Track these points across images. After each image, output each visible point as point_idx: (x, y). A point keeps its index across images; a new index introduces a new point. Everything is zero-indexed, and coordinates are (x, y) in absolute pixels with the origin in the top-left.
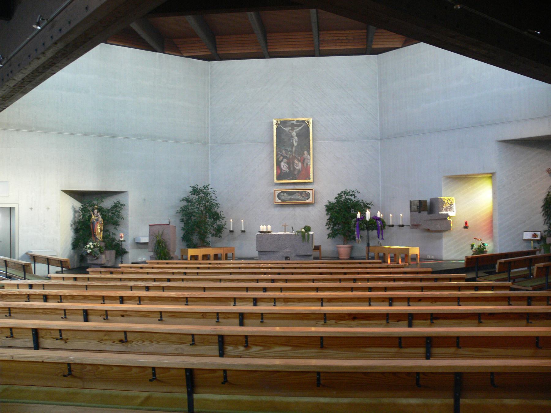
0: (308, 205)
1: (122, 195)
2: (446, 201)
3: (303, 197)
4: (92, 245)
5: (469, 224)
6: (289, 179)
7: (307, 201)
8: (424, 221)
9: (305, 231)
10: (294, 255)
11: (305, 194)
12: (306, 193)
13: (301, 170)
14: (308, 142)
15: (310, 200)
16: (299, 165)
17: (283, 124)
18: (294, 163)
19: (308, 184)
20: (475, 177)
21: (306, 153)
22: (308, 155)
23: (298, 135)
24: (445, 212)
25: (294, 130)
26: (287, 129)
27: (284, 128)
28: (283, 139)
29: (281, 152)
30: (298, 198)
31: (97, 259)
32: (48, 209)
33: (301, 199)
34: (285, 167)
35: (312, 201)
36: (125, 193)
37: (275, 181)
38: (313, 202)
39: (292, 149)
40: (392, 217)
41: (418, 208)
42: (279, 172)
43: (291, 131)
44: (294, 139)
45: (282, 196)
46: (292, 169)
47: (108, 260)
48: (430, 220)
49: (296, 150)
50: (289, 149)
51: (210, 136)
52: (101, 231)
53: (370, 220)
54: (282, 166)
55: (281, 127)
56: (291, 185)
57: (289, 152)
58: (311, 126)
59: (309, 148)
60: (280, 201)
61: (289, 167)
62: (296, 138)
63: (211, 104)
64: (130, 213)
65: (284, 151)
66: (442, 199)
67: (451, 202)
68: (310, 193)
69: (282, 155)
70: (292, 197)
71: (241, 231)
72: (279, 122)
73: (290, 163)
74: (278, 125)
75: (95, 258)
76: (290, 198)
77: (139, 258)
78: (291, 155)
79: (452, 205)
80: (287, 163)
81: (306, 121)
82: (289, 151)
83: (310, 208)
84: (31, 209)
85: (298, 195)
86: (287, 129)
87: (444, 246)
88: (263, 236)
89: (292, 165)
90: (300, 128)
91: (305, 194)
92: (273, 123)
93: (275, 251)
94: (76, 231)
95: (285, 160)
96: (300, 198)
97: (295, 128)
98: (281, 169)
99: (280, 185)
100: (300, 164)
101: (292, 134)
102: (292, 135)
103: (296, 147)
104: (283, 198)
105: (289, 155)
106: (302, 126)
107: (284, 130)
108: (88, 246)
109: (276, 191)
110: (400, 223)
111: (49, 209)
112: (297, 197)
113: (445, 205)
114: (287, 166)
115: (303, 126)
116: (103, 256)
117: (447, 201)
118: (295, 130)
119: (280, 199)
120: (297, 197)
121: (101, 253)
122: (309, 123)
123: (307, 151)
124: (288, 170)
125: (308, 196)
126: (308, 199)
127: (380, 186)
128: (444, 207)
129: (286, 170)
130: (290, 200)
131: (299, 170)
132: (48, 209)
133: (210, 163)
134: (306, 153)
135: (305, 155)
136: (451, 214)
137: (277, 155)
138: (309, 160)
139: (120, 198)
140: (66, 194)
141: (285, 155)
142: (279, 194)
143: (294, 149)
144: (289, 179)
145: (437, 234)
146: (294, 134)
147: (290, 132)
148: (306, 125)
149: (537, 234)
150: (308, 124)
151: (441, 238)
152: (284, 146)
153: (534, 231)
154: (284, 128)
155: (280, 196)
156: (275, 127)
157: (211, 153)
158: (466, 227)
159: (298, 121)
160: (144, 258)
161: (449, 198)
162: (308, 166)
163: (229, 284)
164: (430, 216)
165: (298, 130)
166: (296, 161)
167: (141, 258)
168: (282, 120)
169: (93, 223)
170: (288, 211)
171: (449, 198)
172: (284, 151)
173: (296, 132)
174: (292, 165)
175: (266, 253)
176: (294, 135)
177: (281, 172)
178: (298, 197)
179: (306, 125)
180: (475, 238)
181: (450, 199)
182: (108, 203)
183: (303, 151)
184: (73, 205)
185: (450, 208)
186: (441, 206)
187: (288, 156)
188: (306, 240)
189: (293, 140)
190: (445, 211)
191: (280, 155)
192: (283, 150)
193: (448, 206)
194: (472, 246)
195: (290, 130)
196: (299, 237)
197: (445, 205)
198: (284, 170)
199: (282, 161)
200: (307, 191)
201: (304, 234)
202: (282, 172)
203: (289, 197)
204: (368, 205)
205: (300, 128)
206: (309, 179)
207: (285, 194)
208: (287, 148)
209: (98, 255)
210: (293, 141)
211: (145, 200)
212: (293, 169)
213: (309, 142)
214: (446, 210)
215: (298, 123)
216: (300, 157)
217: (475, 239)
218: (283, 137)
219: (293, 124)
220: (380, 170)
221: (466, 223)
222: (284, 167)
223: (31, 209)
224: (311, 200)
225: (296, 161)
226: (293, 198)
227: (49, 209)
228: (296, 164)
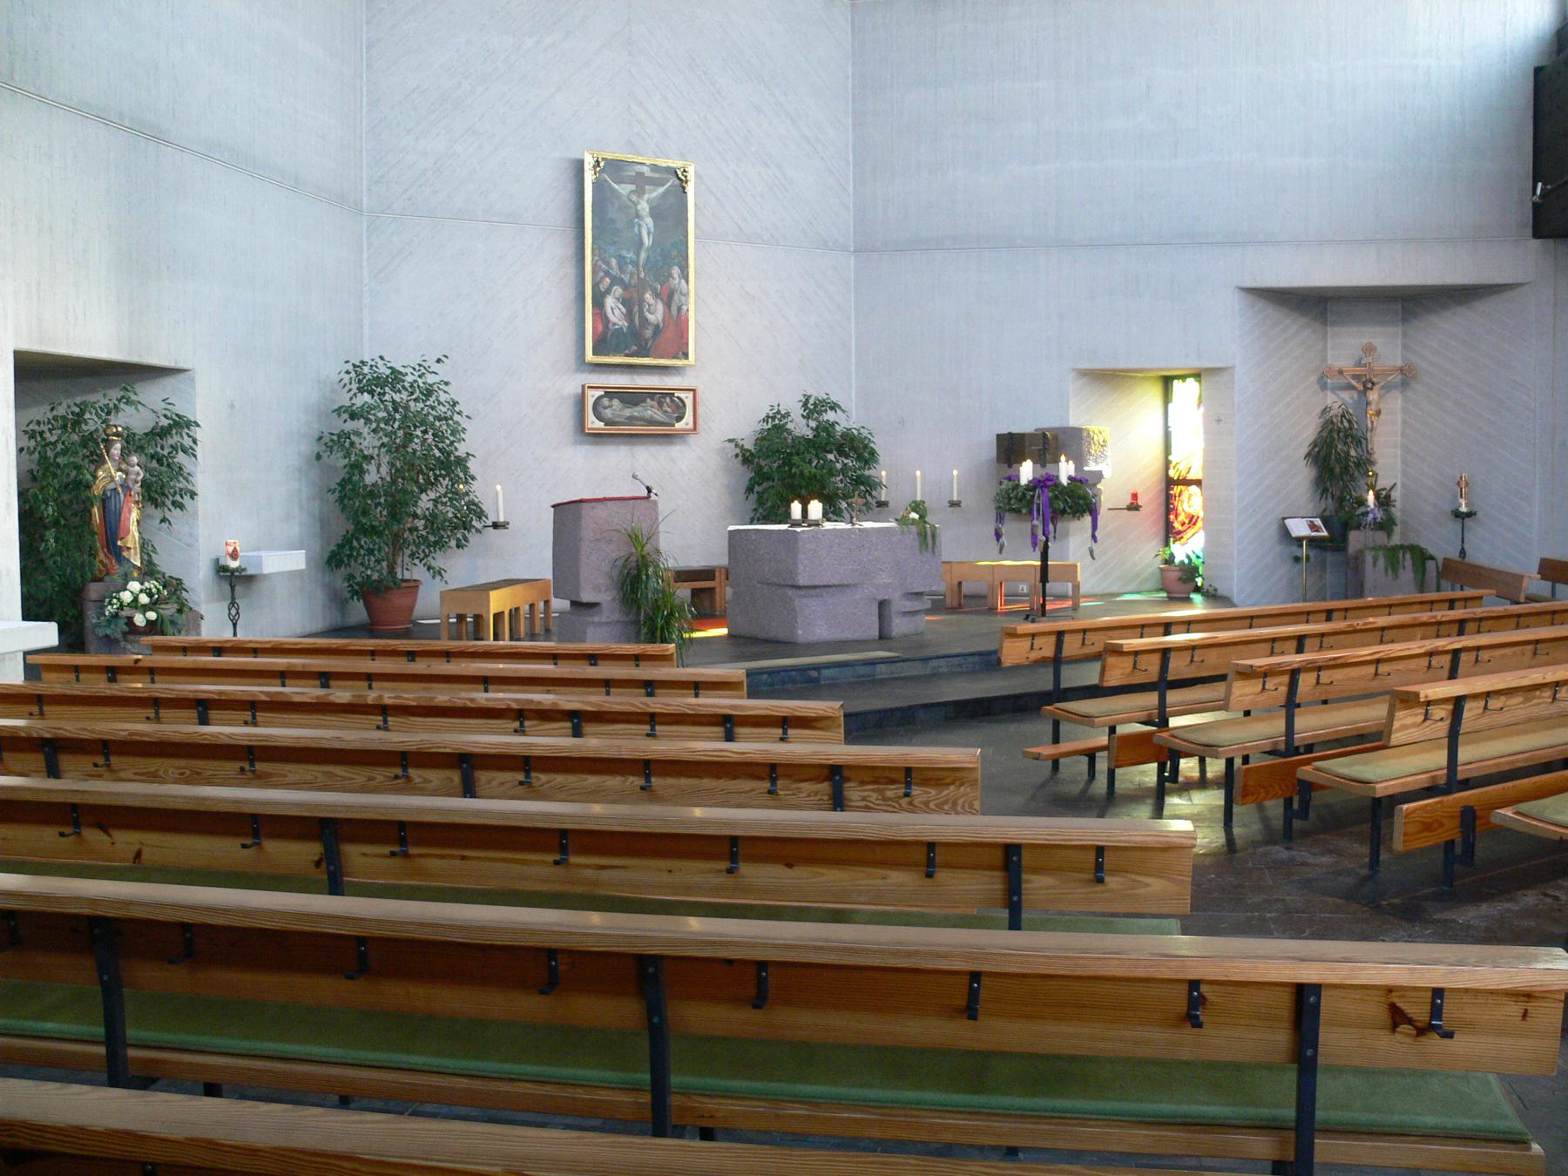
0: (669, 438)
3: (666, 412)
7: (678, 425)
21: (676, 271)
22: (683, 281)
23: (655, 213)
26: (624, 189)
28: (612, 221)
29: (608, 264)
30: (651, 417)
36: (182, 376)
37: (590, 356)
39: (638, 255)
43: (634, 198)
45: (605, 408)
49: (648, 259)
50: (630, 255)
55: (606, 181)
58: (690, 189)
60: (601, 425)
62: (649, 221)
70: (636, 411)
83: (675, 450)
86: (624, 189)
90: (661, 190)
95: (617, 290)
97: (647, 187)
99: (592, 372)
100: (660, 307)
101: (639, 207)
102: (637, 211)
104: (608, 413)
114: (624, 310)
118: (646, 196)
119: (599, 417)
122: (686, 177)
126: (679, 419)
130: (631, 420)
131: (657, 326)
134: (676, 271)
137: (594, 272)
138: (687, 295)
143: (643, 255)
146: (644, 207)
147: (631, 200)
152: (615, 243)
155: (602, 410)
159: (654, 168)
166: (648, 296)
175: (818, 590)
179: (677, 182)
183: (670, 267)
187: (626, 278)
191: (602, 274)
198: (615, 324)
199: (608, 291)
205: (661, 190)
206: (686, 356)
207: (616, 402)
208: (624, 253)
210: (640, 232)
215: (657, 175)
225: (648, 296)
226: (636, 414)
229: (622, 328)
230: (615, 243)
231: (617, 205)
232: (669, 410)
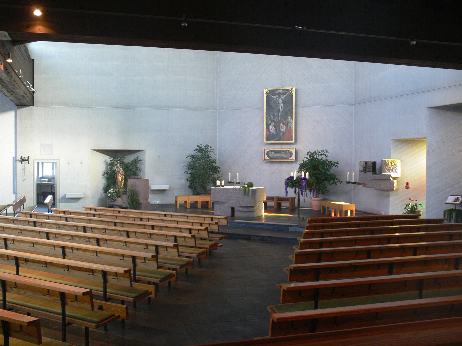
1: (141, 152)
2: (390, 163)
3: (287, 155)
4: (113, 190)
5: (410, 185)
6: (275, 139)
7: (290, 159)
8: (369, 180)
9: (248, 186)
10: (238, 206)
11: (288, 153)
12: (289, 152)
13: (285, 132)
14: (291, 108)
16: (283, 128)
17: (271, 93)
19: (292, 144)
20: (423, 141)
21: (289, 117)
22: (291, 120)
23: (284, 102)
24: (388, 173)
25: (280, 97)
27: (272, 96)
28: (272, 106)
29: (270, 117)
30: (283, 156)
31: (115, 201)
32: (81, 163)
33: (285, 156)
34: (273, 129)
35: (265, 159)
38: (294, 160)
39: (278, 114)
40: (349, 175)
41: (364, 169)
42: (268, 134)
43: (278, 99)
44: (280, 106)
45: (270, 154)
46: (278, 131)
47: (124, 202)
48: (374, 180)
49: (281, 115)
50: (276, 114)
51: (218, 104)
52: (122, 180)
53: (296, 180)
54: (270, 129)
55: (270, 95)
56: (279, 145)
57: (276, 117)
59: (292, 113)
60: (269, 158)
61: (275, 129)
62: (282, 105)
63: (219, 77)
64: (146, 166)
65: (272, 116)
66: (386, 161)
67: (395, 164)
68: (292, 151)
69: (270, 119)
70: (279, 155)
71: (228, 182)
72: (269, 91)
73: (277, 127)
74: (268, 94)
75: (113, 201)
76: (276, 156)
77: (154, 202)
78: (278, 120)
79: (395, 167)
80: (275, 126)
81: (290, 90)
82: (276, 115)
84: (69, 163)
85: (283, 154)
86: (275, 97)
87: (391, 204)
88: (216, 189)
89: (278, 128)
90: (285, 96)
91: (288, 153)
92: (264, 91)
93: (225, 202)
94: (108, 179)
96: (284, 156)
97: (281, 96)
98: (270, 132)
100: (285, 127)
101: (279, 101)
103: (282, 112)
104: (271, 155)
105: (276, 120)
106: (287, 94)
107: (273, 98)
108: (110, 191)
109: (266, 150)
110: (347, 180)
111: (82, 163)
112: (282, 155)
113: (388, 167)
114: (274, 129)
115: (287, 94)
116: (119, 199)
117: (391, 162)
118: (281, 98)
119: (268, 156)
121: (118, 197)
123: (290, 116)
124: (275, 132)
125: (291, 154)
126: (291, 157)
127: (353, 147)
128: (388, 168)
129: (273, 132)
131: (284, 132)
132: (81, 163)
133: (218, 126)
134: (289, 117)
135: (289, 119)
136: (393, 175)
137: (266, 119)
138: (292, 123)
139: (139, 155)
140: (96, 152)
142: (268, 152)
143: (280, 114)
144: (275, 139)
145: (387, 193)
147: (277, 100)
148: (290, 93)
149: (459, 198)
151: (388, 196)
153: (458, 196)
154: (272, 96)
156: (265, 95)
157: (219, 117)
158: (407, 188)
159: (283, 90)
160: (158, 202)
161: (392, 160)
162: (291, 128)
163: (197, 227)
164: (374, 176)
165: (283, 97)
167: (155, 202)
168: (270, 89)
169: (116, 174)
170: (276, 167)
171: (392, 160)
172: (272, 116)
173: (281, 99)
174: (278, 128)
176: (280, 102)
177: (270, 134)
178: (283, 155)
180: (409, 198)
181: (394, 161)
182: (129, 159)
184: (105, 160)
185: (393, 169)
186: (385, 167)
187: (275, 120)
188: (247, 194)
189: (279, 106)
190: (388, 172)
191: (269, 120)
192: (271, 115)
193: (392, 167)
194: (408, 205)
195: (277, 97)
196: (242, 191)
197: (388, 167)
198: (272, 132)
199: (270, 124)
200: (290, 150)
201: (246, 189)
202: (271, 134)
203: (276, 155)
204: (335, 164)
205: (285, 96)
206: (292, 140)
207: (273, 153)
208: (275, 114)
209: (115, 198)
211: (159, 156)
212: (279, 131)
213: (292, 107)
214: (390, 171)
215: (284, 92)
216: (285, 121)
217: (409, 199)
218: (272, 104)
220: (353, 132)
221: (407, 183)
222: (272, 130)
223: (69, 163)
224: (293, 158)
226: (278, 155)
227: (82, 163)
228: (282, 127)
229: (274, 134)
230: (272, 111)
232: (288, 154)
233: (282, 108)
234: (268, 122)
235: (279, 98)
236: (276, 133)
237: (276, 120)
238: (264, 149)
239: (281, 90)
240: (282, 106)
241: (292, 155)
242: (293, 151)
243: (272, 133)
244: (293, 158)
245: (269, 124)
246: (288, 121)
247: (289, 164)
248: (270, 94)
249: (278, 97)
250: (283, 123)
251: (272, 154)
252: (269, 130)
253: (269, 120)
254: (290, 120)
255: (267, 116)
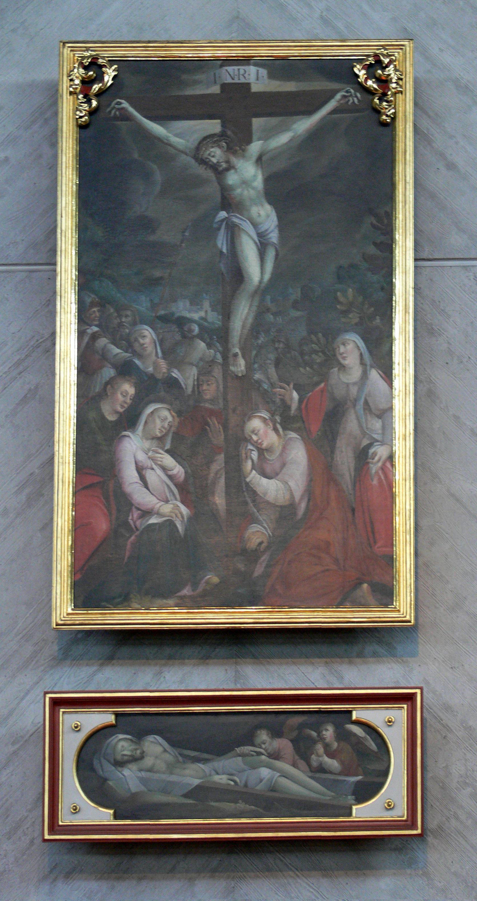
3: (322, 769)
14: (372, 250)
15: (392, 806)
18: (248, 440)
22: (374, 375)
30: (273, 789)
35: (64, 819)
45: (120, 764)
55: (126, 117)
57: (202, 345)
68: (383, 731)
78: (217, 372)
85: (275, 756)
97: (257, 123)
101: (232, 179)
107: (159, 139)
114: (178, 470)
120: (265, 772)
122: (384, 82)
124: (184, 510)
129: (167, 509)
135: (342, 368)
141: (163, 364)
142: (301, 727)
147: (203, 162)
150: (383, 97)
152: (156, 282)
162: (374, 468)
165: (284, 138)
173: (259, 160)
176: (245, 183)
191: (109, 372)
198: (146, 513)
202: (131, 530)
215: (290, 87)
216: (298, 388)
219: (247, 86)
222: (146, 485)
224: (389, 808)
226: (222, 779)
229: (170, 524)
230: (156, 282)
231: (158, 177)
232: (333, 764)
233: (271, 255)
234: (103, 394)
235: (230, 149)
236: (193, 519)
237: (198, 385)
238: (56, 703)
239: (252, 69)
240: (261, 235)
241: (385, 773)
242: (390, 723)
243: (153, 520)
244: (76, 810)
245: (111, 418)
246: (339, 393)
247: (325, 883)
248: (125, 104)
249: (223, 135)
250: (287, 407)
251: (148, 762)
252: (119, 486)
253: (109, 372)
254: (356, 373)
255: (94, 337)
